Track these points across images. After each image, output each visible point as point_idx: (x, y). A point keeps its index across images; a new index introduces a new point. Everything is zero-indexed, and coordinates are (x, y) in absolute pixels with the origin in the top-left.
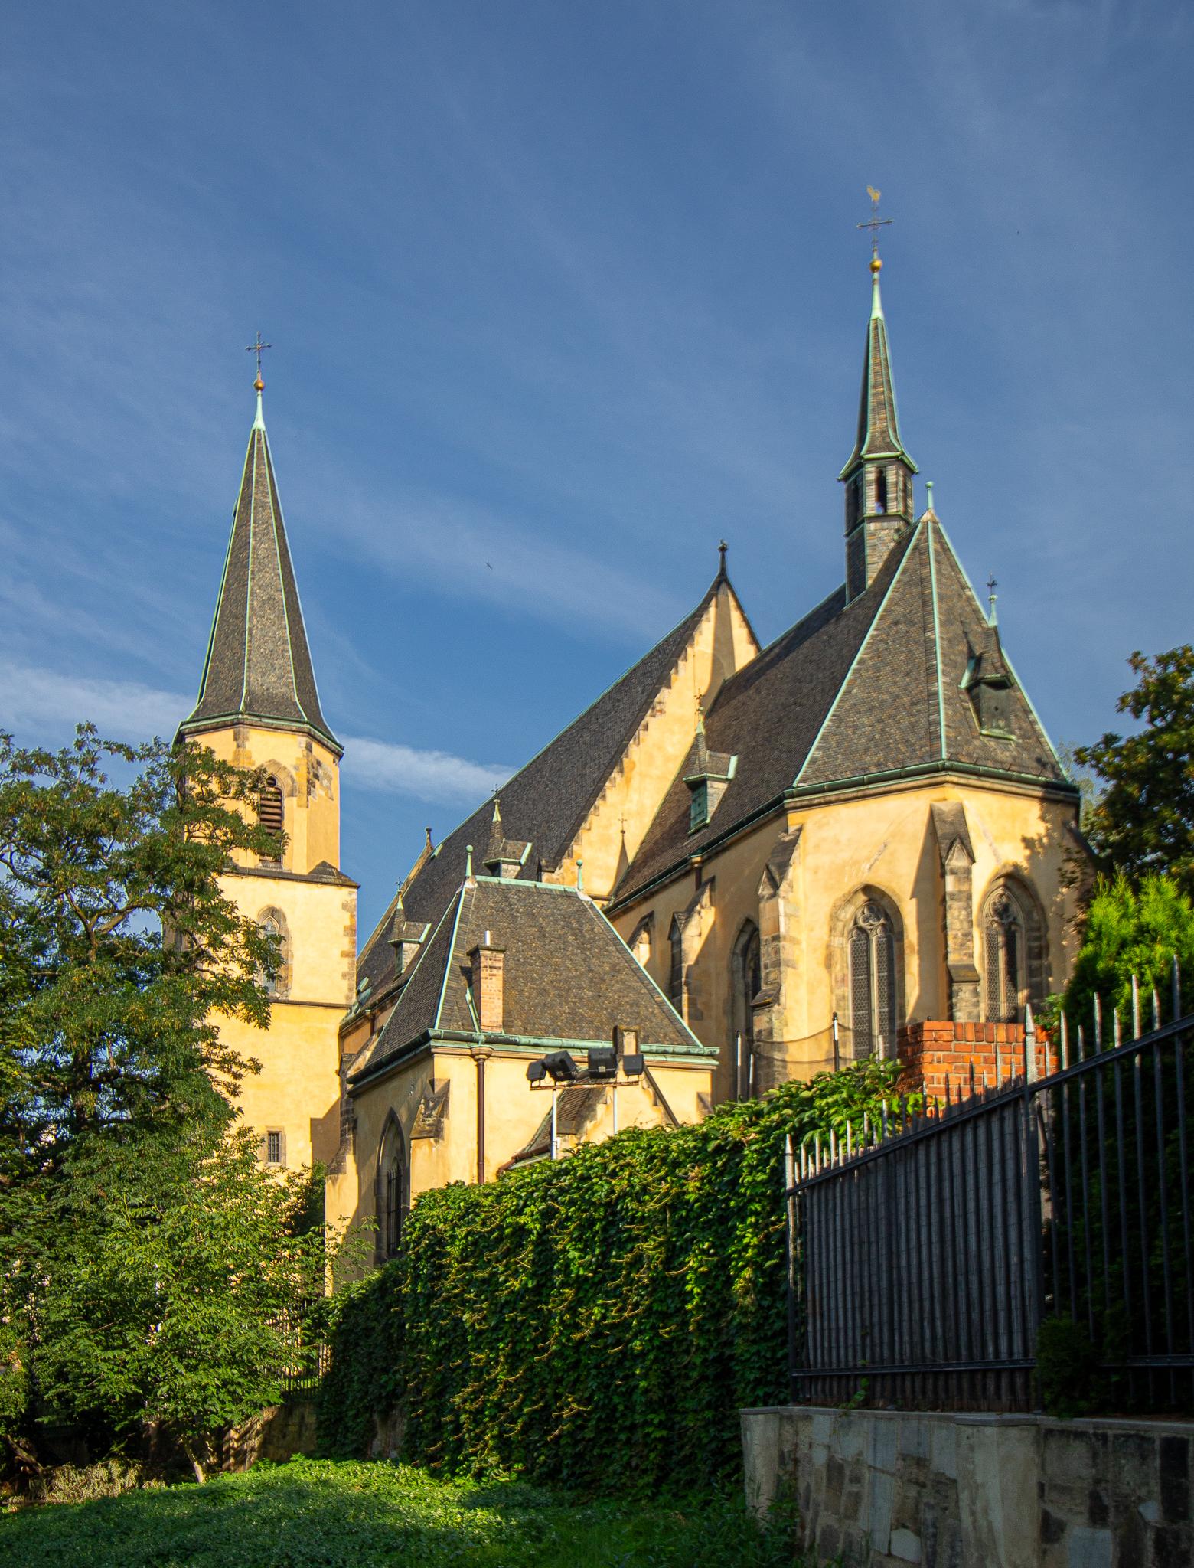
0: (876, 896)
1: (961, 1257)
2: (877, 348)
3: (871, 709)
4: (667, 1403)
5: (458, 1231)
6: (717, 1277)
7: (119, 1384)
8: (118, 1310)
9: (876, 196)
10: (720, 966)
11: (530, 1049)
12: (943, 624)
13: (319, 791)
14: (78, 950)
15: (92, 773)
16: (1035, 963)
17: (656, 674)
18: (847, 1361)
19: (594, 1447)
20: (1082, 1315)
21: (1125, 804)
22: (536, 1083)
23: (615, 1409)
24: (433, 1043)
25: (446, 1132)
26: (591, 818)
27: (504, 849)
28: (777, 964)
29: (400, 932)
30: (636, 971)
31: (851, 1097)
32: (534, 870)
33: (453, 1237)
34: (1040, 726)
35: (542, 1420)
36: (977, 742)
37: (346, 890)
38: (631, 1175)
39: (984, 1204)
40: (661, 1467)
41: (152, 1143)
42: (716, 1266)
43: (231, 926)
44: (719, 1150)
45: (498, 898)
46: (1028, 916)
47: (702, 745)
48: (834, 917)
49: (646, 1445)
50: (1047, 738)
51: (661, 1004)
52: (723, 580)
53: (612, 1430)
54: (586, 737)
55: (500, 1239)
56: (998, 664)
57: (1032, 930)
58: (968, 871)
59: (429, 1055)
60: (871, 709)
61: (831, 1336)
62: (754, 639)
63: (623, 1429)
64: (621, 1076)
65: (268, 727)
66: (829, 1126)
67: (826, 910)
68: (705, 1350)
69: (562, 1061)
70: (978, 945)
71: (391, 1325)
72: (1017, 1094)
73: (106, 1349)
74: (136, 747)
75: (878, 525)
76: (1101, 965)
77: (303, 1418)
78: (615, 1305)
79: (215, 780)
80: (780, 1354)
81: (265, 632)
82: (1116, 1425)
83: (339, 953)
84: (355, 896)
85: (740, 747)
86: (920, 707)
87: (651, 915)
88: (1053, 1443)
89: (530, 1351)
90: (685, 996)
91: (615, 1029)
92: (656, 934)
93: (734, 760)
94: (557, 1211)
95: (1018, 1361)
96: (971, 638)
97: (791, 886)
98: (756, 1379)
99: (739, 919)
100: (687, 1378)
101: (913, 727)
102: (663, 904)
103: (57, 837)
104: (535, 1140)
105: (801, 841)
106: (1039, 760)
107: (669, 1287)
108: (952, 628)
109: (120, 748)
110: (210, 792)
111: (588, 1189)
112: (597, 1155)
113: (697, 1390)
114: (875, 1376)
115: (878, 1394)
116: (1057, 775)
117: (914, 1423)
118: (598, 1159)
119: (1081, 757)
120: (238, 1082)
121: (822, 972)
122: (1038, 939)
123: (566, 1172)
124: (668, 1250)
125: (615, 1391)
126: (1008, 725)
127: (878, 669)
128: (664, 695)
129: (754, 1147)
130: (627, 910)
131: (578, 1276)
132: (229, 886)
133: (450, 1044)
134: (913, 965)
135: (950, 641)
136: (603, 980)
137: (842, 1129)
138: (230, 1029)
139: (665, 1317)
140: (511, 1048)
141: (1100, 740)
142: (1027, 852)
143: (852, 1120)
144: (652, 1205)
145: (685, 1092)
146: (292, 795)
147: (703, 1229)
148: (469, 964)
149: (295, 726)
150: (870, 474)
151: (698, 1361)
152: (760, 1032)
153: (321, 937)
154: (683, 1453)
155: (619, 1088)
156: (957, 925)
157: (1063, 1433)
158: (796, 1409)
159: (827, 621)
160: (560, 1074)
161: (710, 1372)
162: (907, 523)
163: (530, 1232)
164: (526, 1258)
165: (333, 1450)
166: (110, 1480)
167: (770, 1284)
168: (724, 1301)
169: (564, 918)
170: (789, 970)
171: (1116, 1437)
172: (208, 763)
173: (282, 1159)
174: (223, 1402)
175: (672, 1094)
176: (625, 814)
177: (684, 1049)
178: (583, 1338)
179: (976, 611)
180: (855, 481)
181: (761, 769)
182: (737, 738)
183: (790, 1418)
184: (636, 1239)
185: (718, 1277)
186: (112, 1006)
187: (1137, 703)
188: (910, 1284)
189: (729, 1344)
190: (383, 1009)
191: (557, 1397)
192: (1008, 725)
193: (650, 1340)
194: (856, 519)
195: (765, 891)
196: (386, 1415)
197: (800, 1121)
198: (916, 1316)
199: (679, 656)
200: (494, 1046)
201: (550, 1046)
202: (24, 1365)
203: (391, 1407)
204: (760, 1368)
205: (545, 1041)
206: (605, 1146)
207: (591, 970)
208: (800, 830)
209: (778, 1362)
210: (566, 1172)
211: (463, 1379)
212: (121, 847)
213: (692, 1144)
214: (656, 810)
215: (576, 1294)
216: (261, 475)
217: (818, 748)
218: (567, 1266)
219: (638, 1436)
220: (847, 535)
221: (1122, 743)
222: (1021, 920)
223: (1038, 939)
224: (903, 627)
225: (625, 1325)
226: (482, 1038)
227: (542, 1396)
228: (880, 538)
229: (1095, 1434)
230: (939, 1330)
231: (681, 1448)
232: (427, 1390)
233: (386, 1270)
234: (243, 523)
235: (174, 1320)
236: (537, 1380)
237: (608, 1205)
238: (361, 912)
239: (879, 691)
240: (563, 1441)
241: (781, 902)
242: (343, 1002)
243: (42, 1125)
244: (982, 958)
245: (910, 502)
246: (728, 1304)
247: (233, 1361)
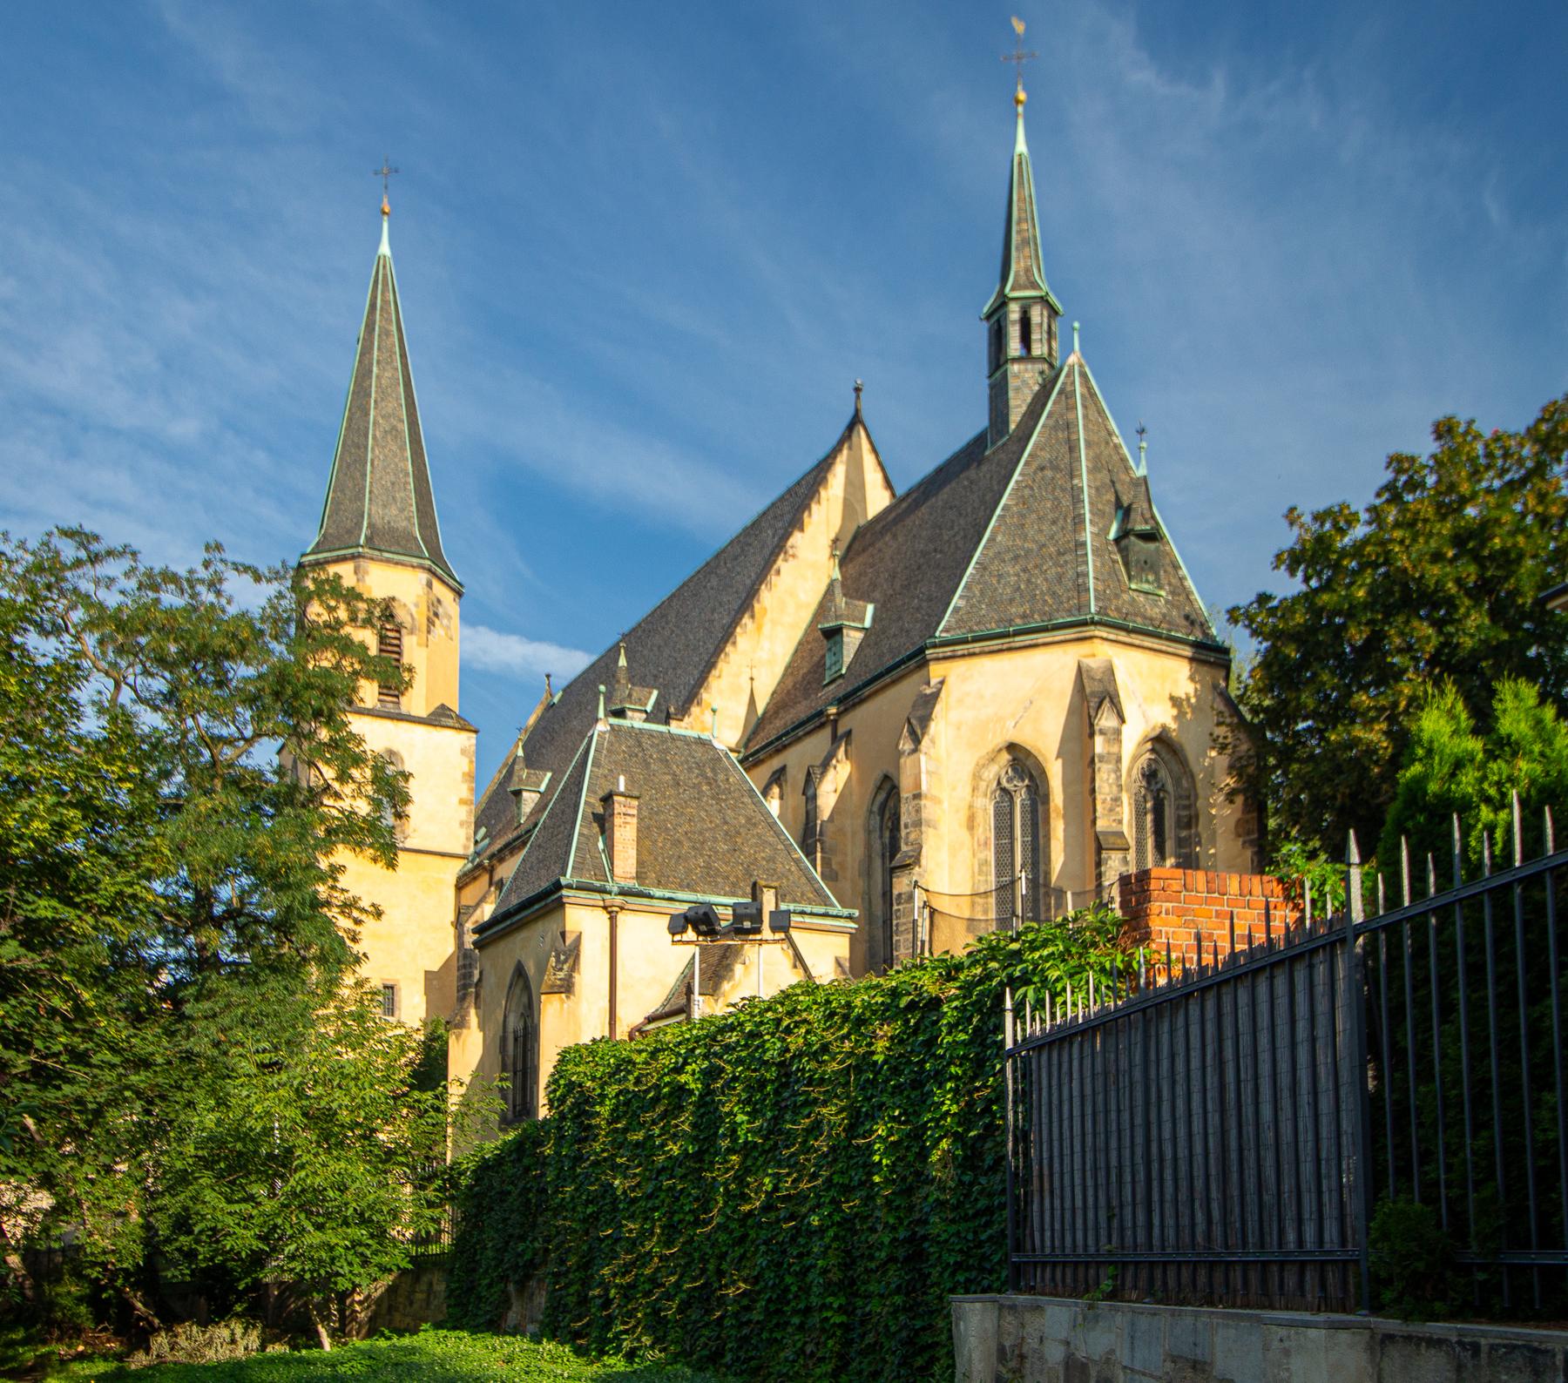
0: (1021, 756)
1: (1249, 1129)
2: (1021, 183)
3: (1016, 558)
4: (848, 1286)
5: (608, 1090)
6: (908, 1148)
7: (244, 1240)
8: (241, 1159)
9: (1019, 27)
10: (855, 825)
11: (664, 903)
12: (1089, 472)
13: (438, 630)
14: (207, 776)
15: (218, 593)
16: (1184, 834)
17: (787, 517)
18: (1086, 1246)
19: (762, 1330)
20: (1429, 1199)
21: (1281, 666)
22: (678, 937)
23: (787, 1289)
24: (565, 892)
25: (577, 988)
26: (721, 665)
27: (630, 695)
28: (918, 824)
29: (521, 780)
30: (772, 825)
31: (1068, 950)
32: (662, 714)
33: (603, 1096)
34: (1189, 583)
35: (705, 1297)
36: (1125, 597)
37: (465, 735)
38: (808, 1032)
39: (1284, 1066)
40: (840, 1356)
41: (273, 984)
42: (908, 1135)
43: (358, 760)
44: (912, 1006)
45: (631, 742)
46: (1177, 783)
47: (838, 591)
48: (977, 777)
49: (823, 1330)
50: (1196, 595)
51: (797, 862)
52: (856, 421)
53: (783, 1313)
54: (714, 582)
55: (656, 1100)
56: (1148, 516)
57: (1180, 797)
58: (1118, 732)
59: (560, 905)
60: (1016, 558)
61: (1061, 1217)
62: (888, 484)
63: (795, 1312)
64: (767, 933)
65: (388, 561)
66: (1044, 980)
67: (969, 768)
68: (894, 1228)
69: (705, 914)
70: (1126, 812)
71: (530, 1190)
72: (1338, 933)
73: (229, 1201)
74: (263, 570)
75: (1022, 367)
76: (1433, 787)
77: (431, 1284)
78: (788, 1175)
79: (343, 606)
80: (984, 1237)
81: (387, 463)
82: (1489, 1333)
83: (456, 801)
84: (474, 741)
85: (877, 595)
86: (1068, 557)
87: (783, 769)
88: (1393, 1351)
89: (689, 1223)
90: (819, 855)
91: (755, 884)
92: (788, 789)
93: (870, 608)
94: (723, 1070)
95: (1330, 1252)
96: (1118, 486)
97: (933, 741)
98: (956, 1263)
99: (876, 776)
100: (871, 1258)
101: (1060, 578)
102: (796, 758)
103: (185, 658)
104: (668, 1000)
105: (942, 695)
106: (1187, 617)
107: (852, 1157)
108: (1099, 476)
109: (247, 569)
110: (337, 620)
111: (758, 1047)
112: (767, 1010)
113: (884, 1273)
114: (1125, 1264)
115: (1129, 1284)
116: (1206, 634)
117: (1189, 1320)
118: (769, 1014)
119: (1233, 615)
120: (358, 928)
121: (965, 834)
122: (1188, 807)
123: (732, 1028)
124: (850, 1117)
125: (788, 1270)
126: (1158, 580)
127: (1023, 516)
128: (796, 539)
129: (954, 1004)
130: (761, 762)
131: (746, 1142)
132: (357, 724)
133: (582, 894)
134: (1058, 828)
135: (1097, 489)
136: (738, 833)
137: (1059, 986)
138: (357, 873)
139: (847, 1190)
140: (645, 901)
141: (1253, 598)
142: (1175, 712)
143: (1071, 976)
144: (835, 1066)
145: (826, 952)
146: (412, 633)
147: (892, 1094)
148: (601, 811)
149: (415, 561)
150: (1014, 312)
151: (887, 1240)
152: (900, 895)
153: (442, 783)
154: (867, 1341)
155: (765, 946)
156: (1106, 789)
157: (1408, 1338)
158: (1022, 1298)
159: (966, 467)
160: (703, 928)
161: (901, 1253)
162: (1051, 366)
163: (691, 1092)
164: (685, 1122)
165: (465, 1321)
166: (233, 1341)
167: (971, 1158)
168: (918, 1174)
169: (698, 767)
170: (931, 831)
171: (1493, 1348)
172: (334, 588)
173: (397, 1013)
174: (350, 1264)
175: (799, 959)
176: (755, 665)
177: (821, 910)
178: (751, 1211)
179: (1123, 460)
180: (998, 321)
181: (900, 618)
182: (874, 586)
183: (1013, 1308)
184: (815, 1102)
185: (912, 1146)
186: (238, 838)
187: (1293, 560)
188: (1175, 1159)
189: (924, 1222)
190: (501, 860)
191: (720, 1273)
192: (1158, 580)
193: (830, 1215)
194: (998, 360)
195: (905, 745)
196: (522, 1286)
197: (1010, 976)
198: (1183, 1195)
199: (812, 498)
200: (628, 899)
201: (684, 901)
202: (141, 1214)
203: (528, 1277)
204: (961, 1251)
205: (680, 895)
206: (775, 1001)
207: (726, 823)
208: (942, 682)
209: (980, 1245)
210: (732, 1028)
211: (612, 1250)
212: (251, 671)
213: (880, 1000)
214: (787, 659)
215: (742, 1163)
216: (385, 302)
217: (961, 597)
218: (734, 1131)
219: (815, 1319)
221: (1275, 603)
222: (1170, 787)
223: (1188, 807)
224: (1049, 473)
225: (802, 1198)
226: (615, 889)
227: (703, 1271)
228: (1023, 380)
229: (1460, 1343)
230: (1216, 1214)
231: (863, 1336)
232: (572, 1261)
233: (524, 1130)
234: (367, 351)
235: (303, 1174)
236: (696, 1255)
237: (781, 1065)
238: (481, 755)
239: (1025, 540)
240: (727, 1322)
241: (923, 758)
242: (460, 851)
243: (161, 964)
244: (1130, 825)
245: (1054, 344)
246: (922, 1178)
247: (364, 1221)
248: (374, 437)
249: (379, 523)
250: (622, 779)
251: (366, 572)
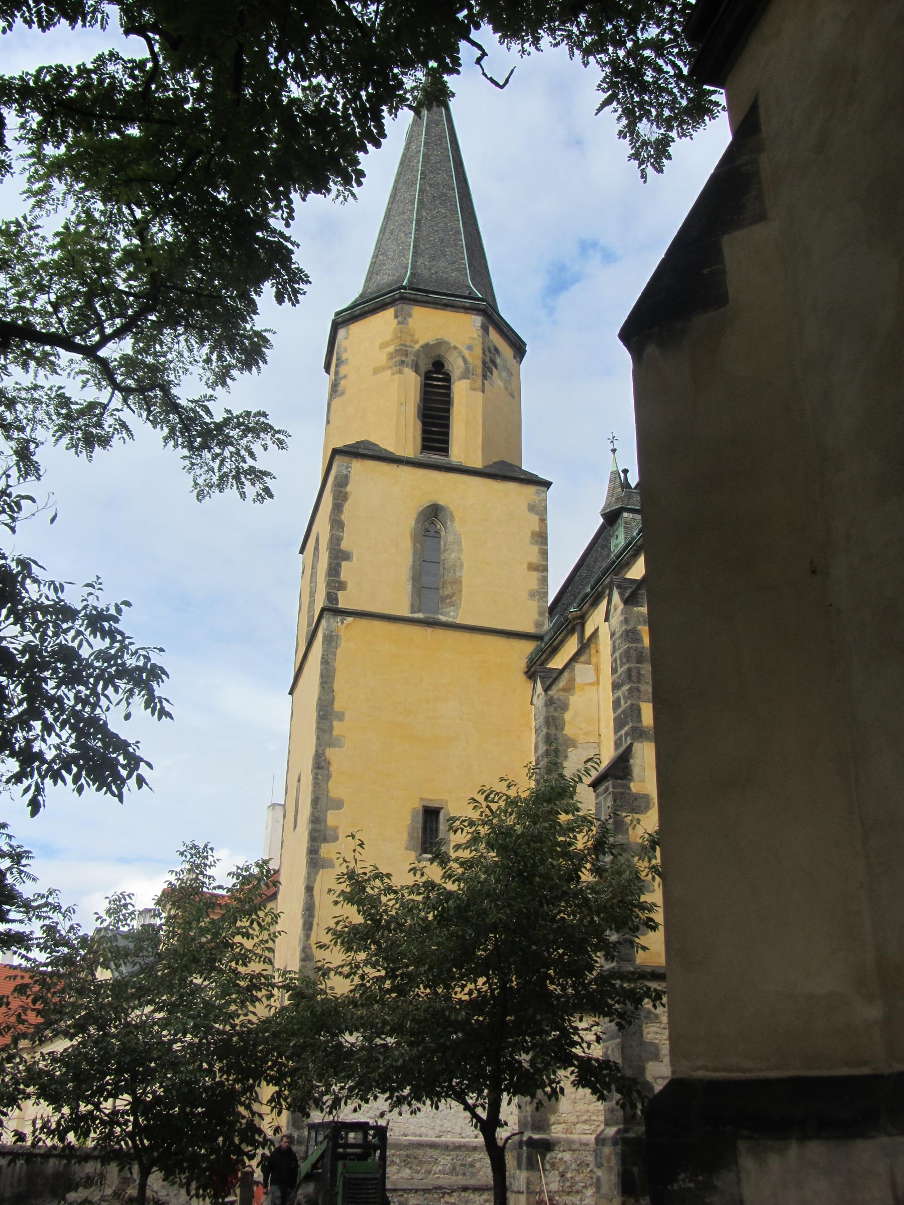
251: (410, 316)
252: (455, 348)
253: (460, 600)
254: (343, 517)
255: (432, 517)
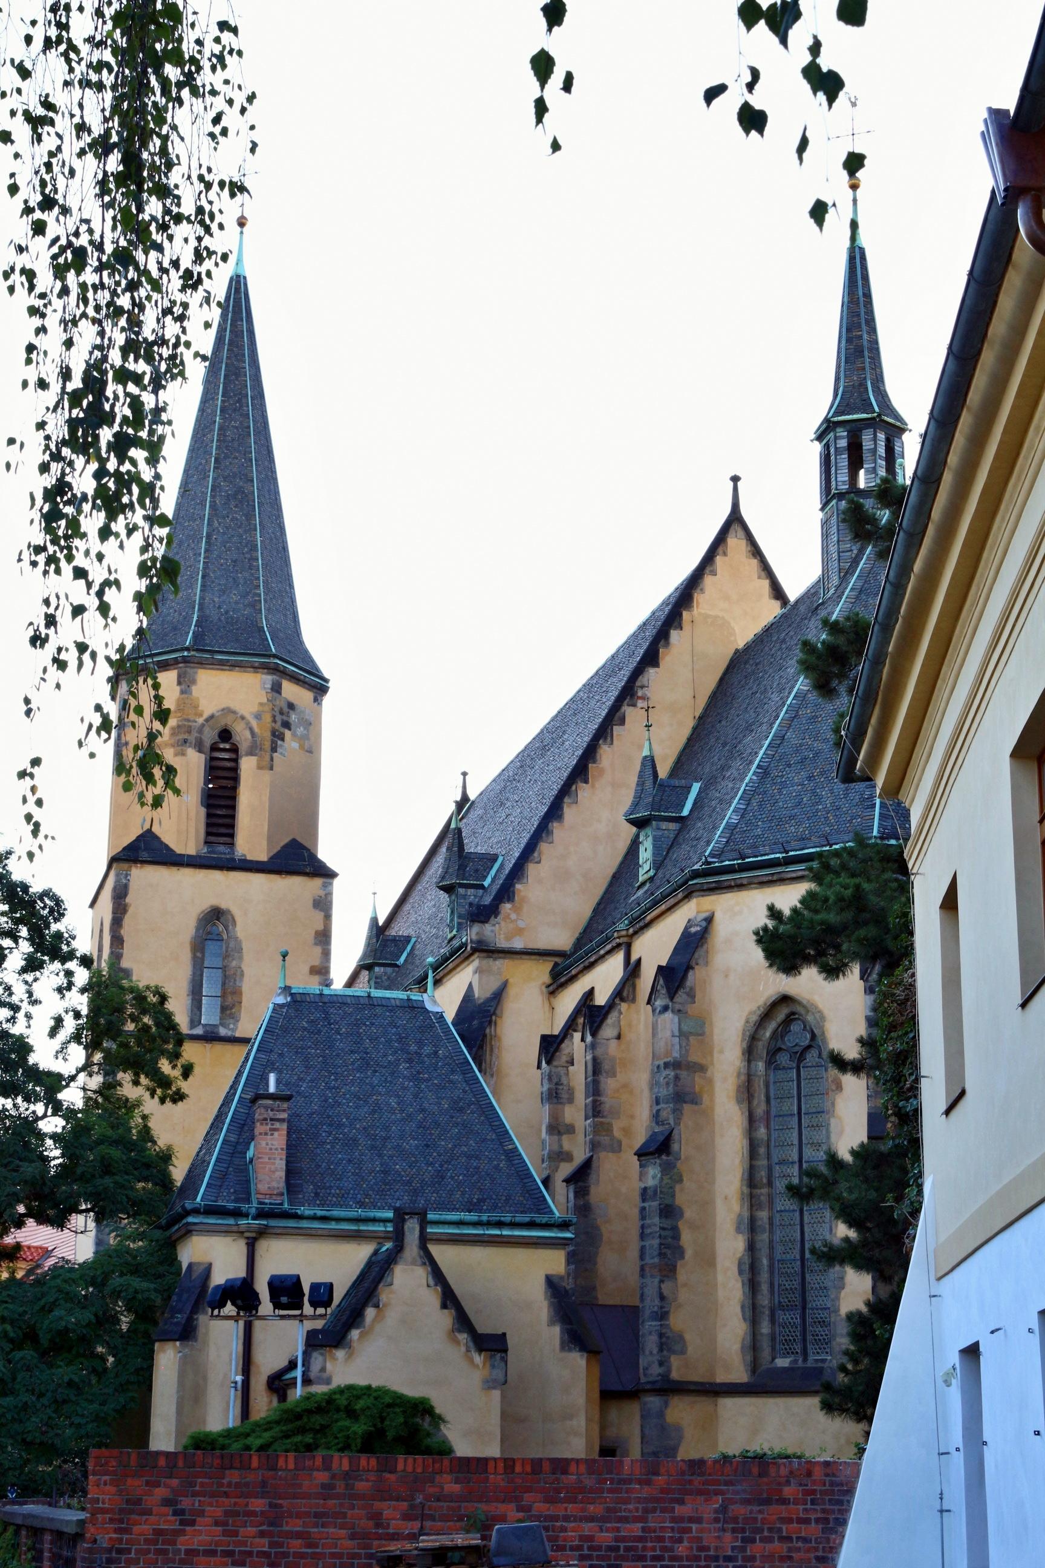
83: (307, 969)
146: (251, 753)
220: (822, 509)
226: (253, 1211)
248: (213, 506)
249: (213, 614)
250: (272, 1078)
251: (194, 682)
252: (243, 718)
253: (240, 1011)
254: (122, 932)
255: (214, 923)
